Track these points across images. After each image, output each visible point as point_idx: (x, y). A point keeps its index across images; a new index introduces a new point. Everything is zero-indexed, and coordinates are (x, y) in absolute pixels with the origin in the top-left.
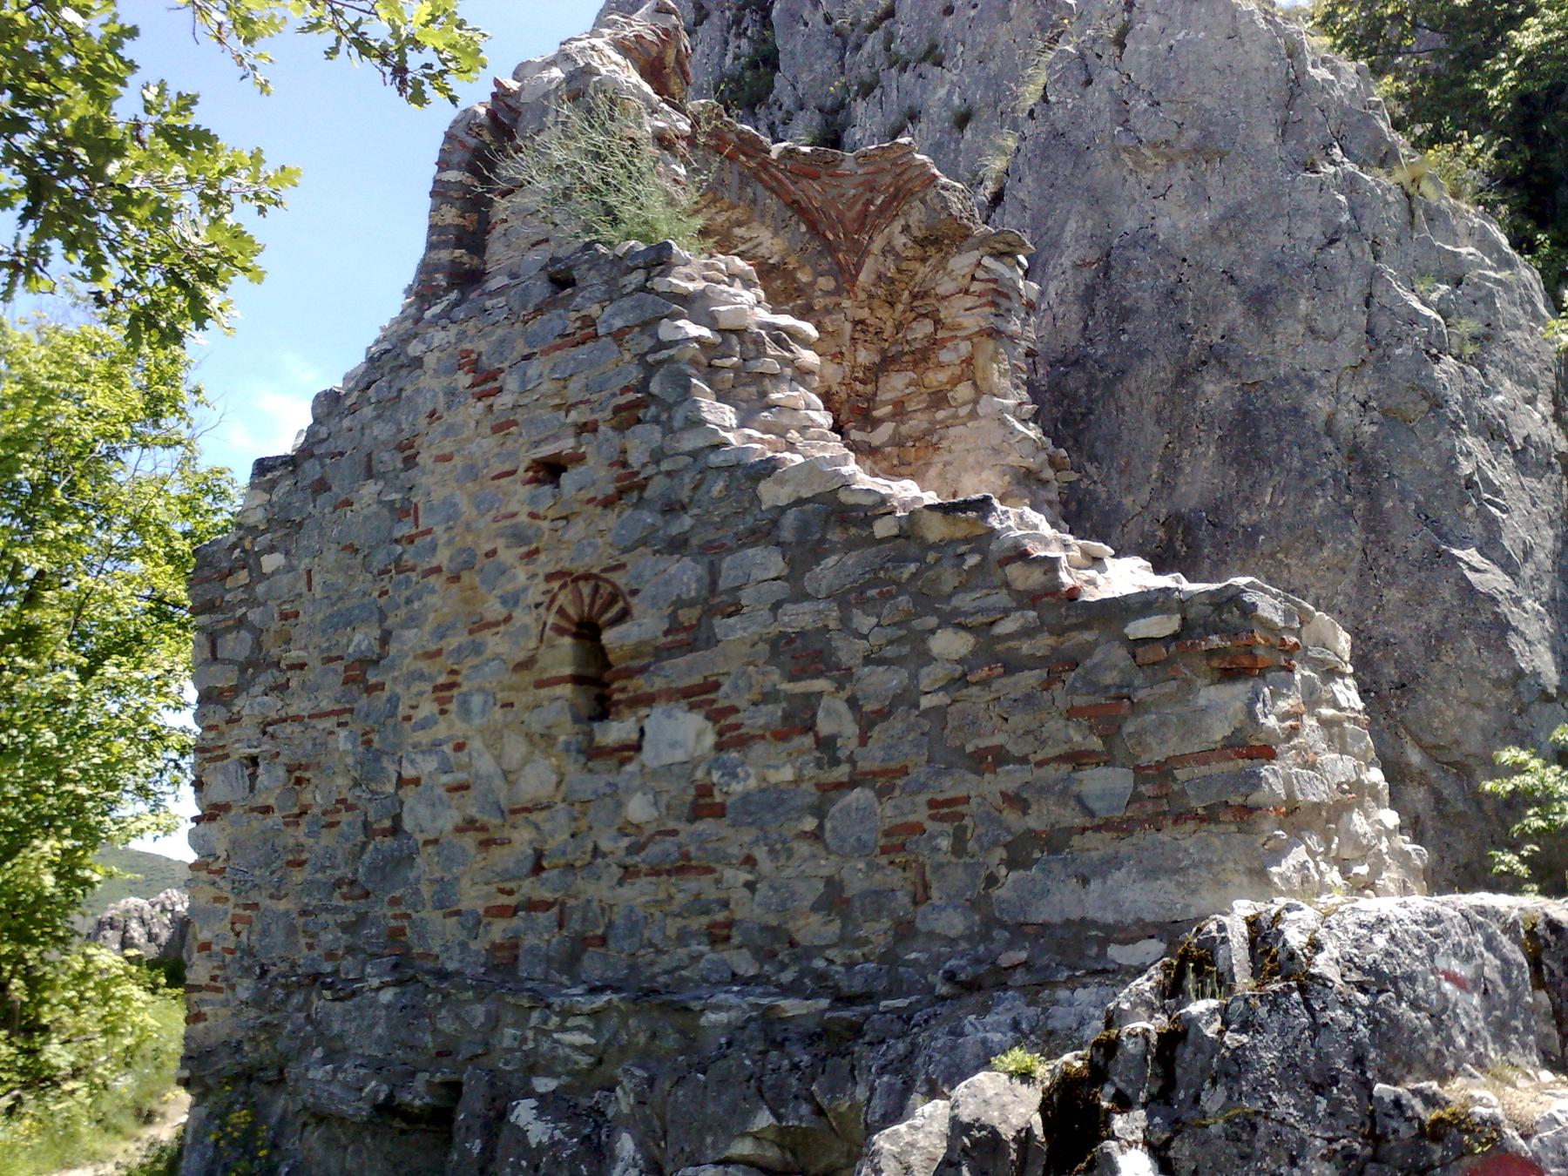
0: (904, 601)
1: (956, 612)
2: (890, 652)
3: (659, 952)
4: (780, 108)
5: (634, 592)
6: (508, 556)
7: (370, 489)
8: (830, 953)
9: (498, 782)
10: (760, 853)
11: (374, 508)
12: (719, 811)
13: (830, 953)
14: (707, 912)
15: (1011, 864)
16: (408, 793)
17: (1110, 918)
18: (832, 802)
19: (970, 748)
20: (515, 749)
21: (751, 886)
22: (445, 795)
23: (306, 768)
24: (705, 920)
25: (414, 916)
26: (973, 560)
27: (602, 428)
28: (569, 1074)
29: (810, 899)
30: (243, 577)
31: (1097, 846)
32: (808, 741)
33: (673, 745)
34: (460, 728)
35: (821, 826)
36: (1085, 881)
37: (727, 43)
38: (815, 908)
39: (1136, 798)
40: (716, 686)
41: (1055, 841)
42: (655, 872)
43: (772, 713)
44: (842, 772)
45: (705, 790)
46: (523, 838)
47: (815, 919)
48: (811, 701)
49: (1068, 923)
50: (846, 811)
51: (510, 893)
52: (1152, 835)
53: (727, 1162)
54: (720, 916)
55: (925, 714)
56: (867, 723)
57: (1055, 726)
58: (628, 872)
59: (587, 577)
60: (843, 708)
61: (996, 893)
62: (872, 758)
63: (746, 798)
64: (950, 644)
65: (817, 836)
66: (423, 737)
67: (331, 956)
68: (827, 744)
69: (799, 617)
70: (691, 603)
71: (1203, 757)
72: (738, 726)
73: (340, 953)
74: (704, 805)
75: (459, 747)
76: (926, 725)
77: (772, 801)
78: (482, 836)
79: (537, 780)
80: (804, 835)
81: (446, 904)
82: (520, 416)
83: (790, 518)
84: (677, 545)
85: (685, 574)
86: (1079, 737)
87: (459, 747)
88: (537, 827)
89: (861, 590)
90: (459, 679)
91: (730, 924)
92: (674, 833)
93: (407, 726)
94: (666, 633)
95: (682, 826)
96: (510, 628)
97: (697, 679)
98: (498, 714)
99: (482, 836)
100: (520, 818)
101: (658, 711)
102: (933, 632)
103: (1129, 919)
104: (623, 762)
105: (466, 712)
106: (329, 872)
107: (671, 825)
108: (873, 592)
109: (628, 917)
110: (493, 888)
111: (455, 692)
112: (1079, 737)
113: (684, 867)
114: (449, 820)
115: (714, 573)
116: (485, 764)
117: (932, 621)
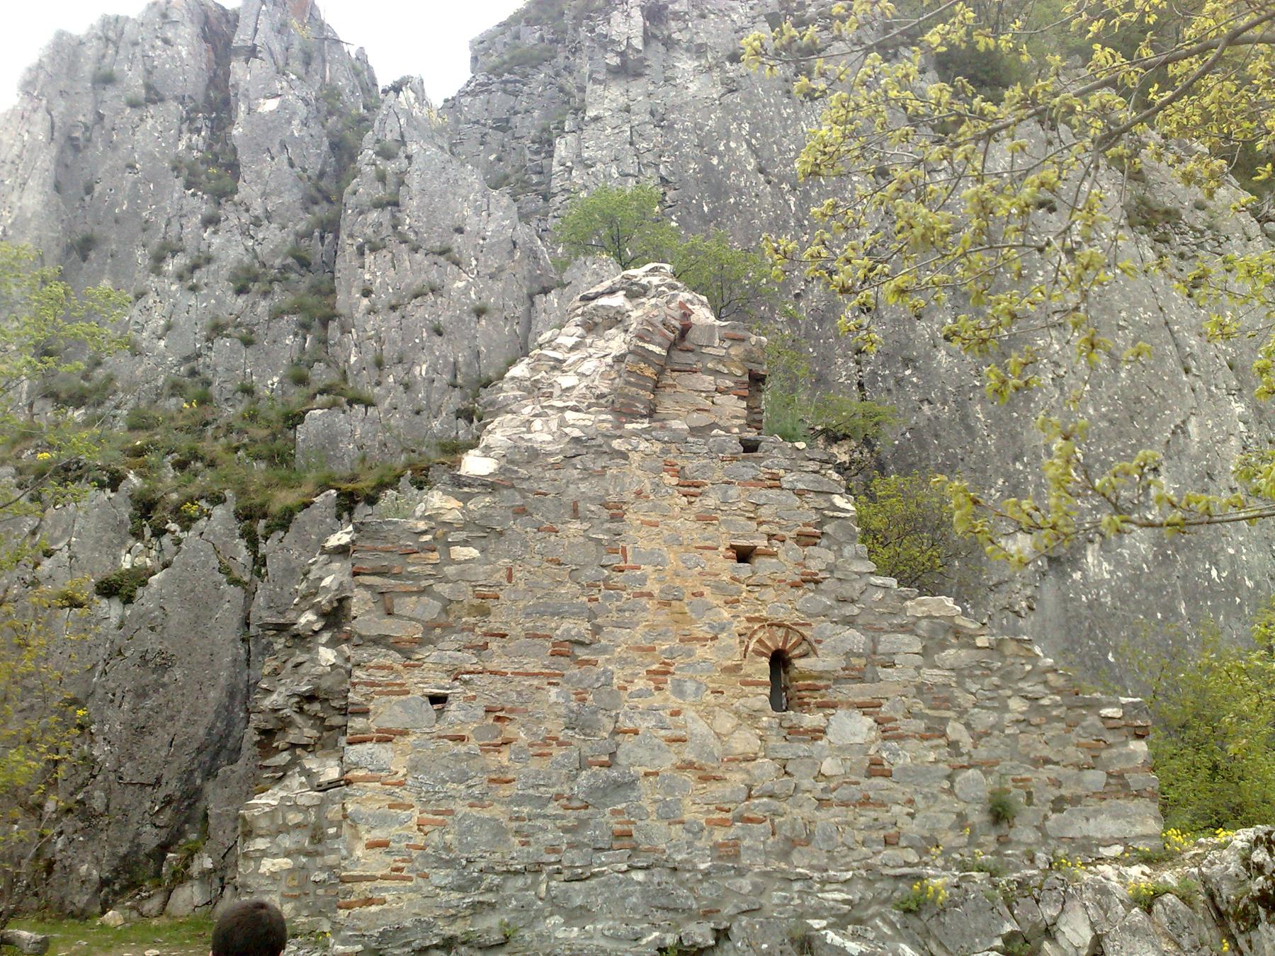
0: (995, 680)
1: (1021, 689)
2: (988, 703)
3: (850, 849)
4: (247, 210)
5: (819, 642)
6: (710, 597)
7: (575, 526)
8: (961, 851)
9: (712, 741)
10: (918, 798)
11: (581, 539)
12: (887, 775)
13: (961, 851)
14: (883, 828)
15: (1054, 811)
16: (627, 742)
17: (1099, 836)
18: (957, 775)
19: (1032, 756)
20: (725, 722)
21: (912, 816)
22: (664, 744)
23: (512, 711)
24: (882, 833)
25: (639, 823)
26: (1028, 668)
27: (788, 541)
28: (833, 916)
29: (948, 824)
30: (434, 557)
31: (1093, 804)
32: (942, 741)
33: (854, 734)
34: (675, 702)
35: (952, 786)
36: (1088, 820)
37: (180, 132)
38: (951, 828)
39: (1107, 784)
40: (880, 706)
41: (1076, 800)
42: (844, 804)
43: (920, 725)
44: (964, 760)
45: (876, 763)
46: (737, 779)
47: (951, 835)
48: (944, 720)
49: (1085, 837)
50: (968, 779)
51: (728, 811)
52: (1115, 801)
53: (991, 950)
54: (892, 831)
55: (1008, 736)
56: (978, 737)
57: (1070, 750)
58: (822, 803)
59: (780, 626)
60: (962, 728)
61: (1048, 823)
62: (982, 753)
63: (904, 769)
64: (1017, 706)
65: (950, 791)
66: (642, 704)
67: (553, 850)
68: (954, 745)
69: (931, 675)
70: (859, 656)
71: (1135, 770)
72: (896, 729)
73: (564, 848)
74: (876, 769)
75: (676, 713)
76: (1008, 741)
77: (914, 774)
78: (701, 773)
79: (744, 741)
80: (943, 791)
81: (670, 815)
82: (719, 515)
83: (924, 623)
84: (849, 622)
85: (855, 638)
86: (1081, 756)
87: (676, 713)
88: (748, 772)
89: (971, 668)
90: (672, 669)
91: (898, 835)
92: (857, 783)
93: (624, 695)
94: (844, 669)
95: (862, 780)
96: (716, 643)
97: (867, 699)
98: (710, 698)
99: (701, 773)
100: (733, 765)
101: (840, 712)
102: (1009, 697)
103: (1108, 836)
104: (815, 739)
105: (679, 691)
106: (542, 789)
107: (853, 778)
108: (978, 672)
109: (824, 830)
110: (712, 808)
111: (669, 678)
112: (1081, 756)
113: (865, 802)
114: (667, 762)
115: (875, 642)
116: (699, 727)
117: (1009, 693)
